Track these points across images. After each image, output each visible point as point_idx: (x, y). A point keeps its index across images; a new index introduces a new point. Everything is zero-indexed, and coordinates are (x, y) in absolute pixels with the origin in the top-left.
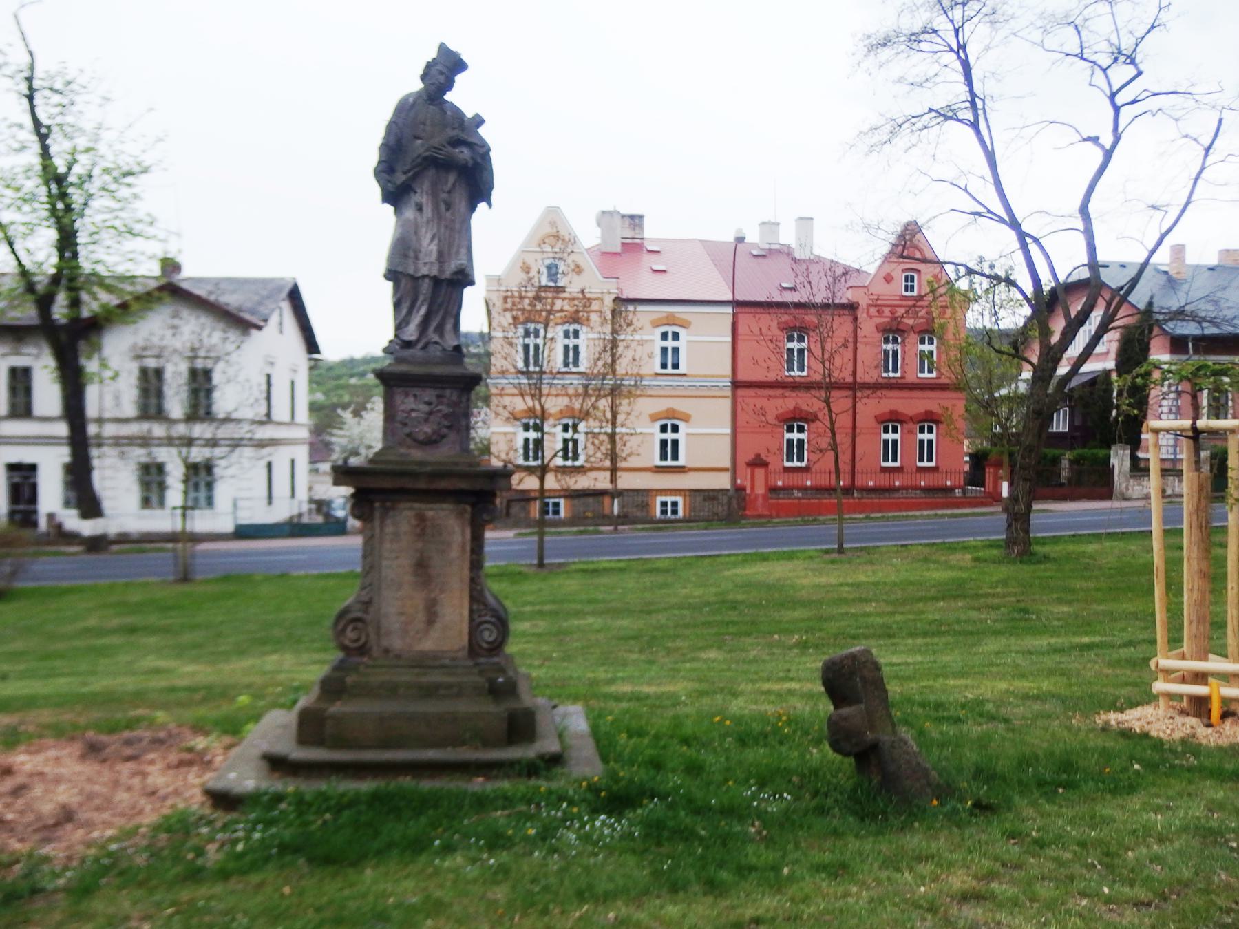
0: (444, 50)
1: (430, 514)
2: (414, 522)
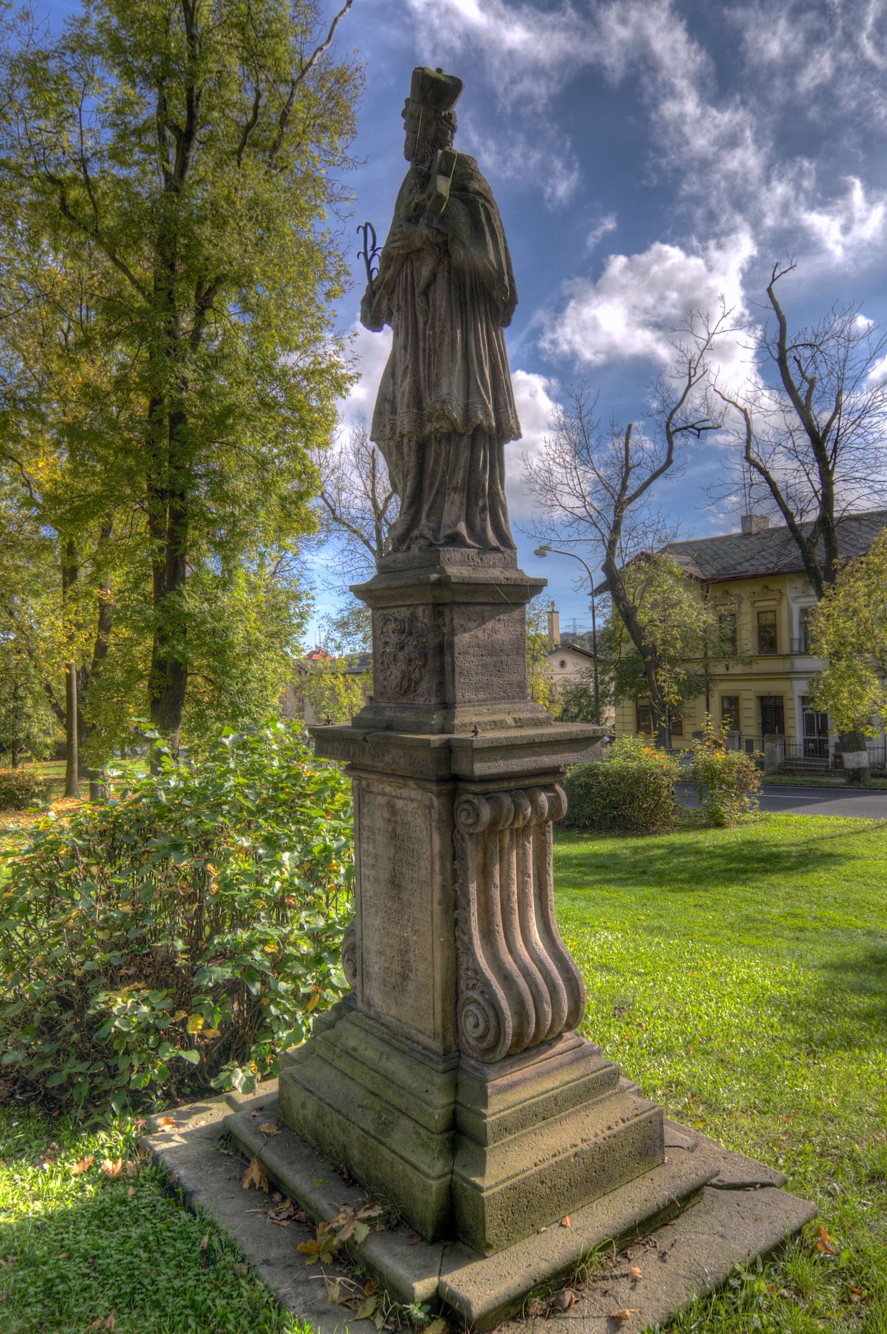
1: (400, 804)
2: (387, 815)
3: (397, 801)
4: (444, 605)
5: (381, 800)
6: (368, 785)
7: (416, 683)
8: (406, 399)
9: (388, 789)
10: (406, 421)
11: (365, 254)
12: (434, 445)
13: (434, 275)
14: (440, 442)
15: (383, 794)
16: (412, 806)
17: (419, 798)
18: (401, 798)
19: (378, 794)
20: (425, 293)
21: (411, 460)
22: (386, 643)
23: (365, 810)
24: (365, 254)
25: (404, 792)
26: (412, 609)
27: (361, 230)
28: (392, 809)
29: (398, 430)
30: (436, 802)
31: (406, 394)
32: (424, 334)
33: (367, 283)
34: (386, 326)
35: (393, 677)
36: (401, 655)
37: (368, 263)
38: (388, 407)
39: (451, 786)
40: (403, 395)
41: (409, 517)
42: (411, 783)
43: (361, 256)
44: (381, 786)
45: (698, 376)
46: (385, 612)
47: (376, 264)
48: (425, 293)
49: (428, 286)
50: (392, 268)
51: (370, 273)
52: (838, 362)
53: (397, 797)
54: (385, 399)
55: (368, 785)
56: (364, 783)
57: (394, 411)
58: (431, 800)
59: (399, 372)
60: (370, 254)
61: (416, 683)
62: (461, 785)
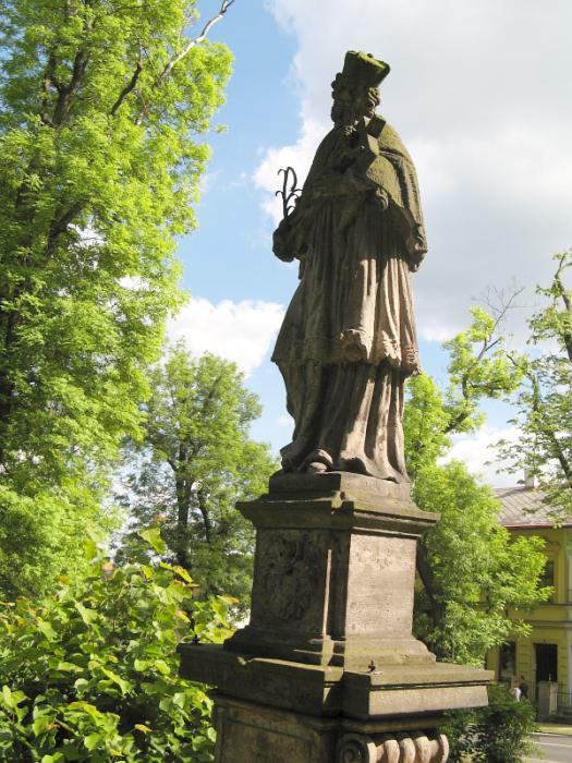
0: (352, 60)
1: (273, 738)
2: (255, 749)
3: (270, 734)
4: (340, 531)
5: (249, 731)
6: (236, 714)
7: (303, 610)
8: (316, 326)
9: (260, 721)
10: (314, 346)
11: (284, 194)
12: (340, 373)
13: (353, 221)
14: (345, 371)
15: (254, 726)
16: (287, 742)
17: (298, 734)
18: (275, 732)
19: (249, 725)
20: (345, 233)
21: (314, 382)
22: (272, 565)
23: (230, 741)
24: (284, 194)
25: (280, 726)
26: (304, 532)
27: (282, 173)
28: (262, 742)
29: (305, 354)
30: (318, 739)
31: (317, 321)
32: (339, 269)
33: (282, 217)
34: (295, 260)
35: (277, 601)
36: (288, 579)
37: (286, 202)
38: (294, 331)
39: (331, 724)
40: (314, 322)
41: (306, 440)
42: (292, 718)
43: (280, 195)
44: (253, 717)
45: (492, 342)
46: (273, 532)
47: (292, 203)
48: (345, 233)
49: (347, 227)
50: (312, 208)
51: (286, 210)
52: (139, 350)
53: (270, 730)
54: (292, 324)
55: (236, 714)
56: (231, 711)
57: (301, 335)
58: (312, 736)
59: (311, 302)
60: (288, 193)
61: (303, 610)
62: (347, 724)
